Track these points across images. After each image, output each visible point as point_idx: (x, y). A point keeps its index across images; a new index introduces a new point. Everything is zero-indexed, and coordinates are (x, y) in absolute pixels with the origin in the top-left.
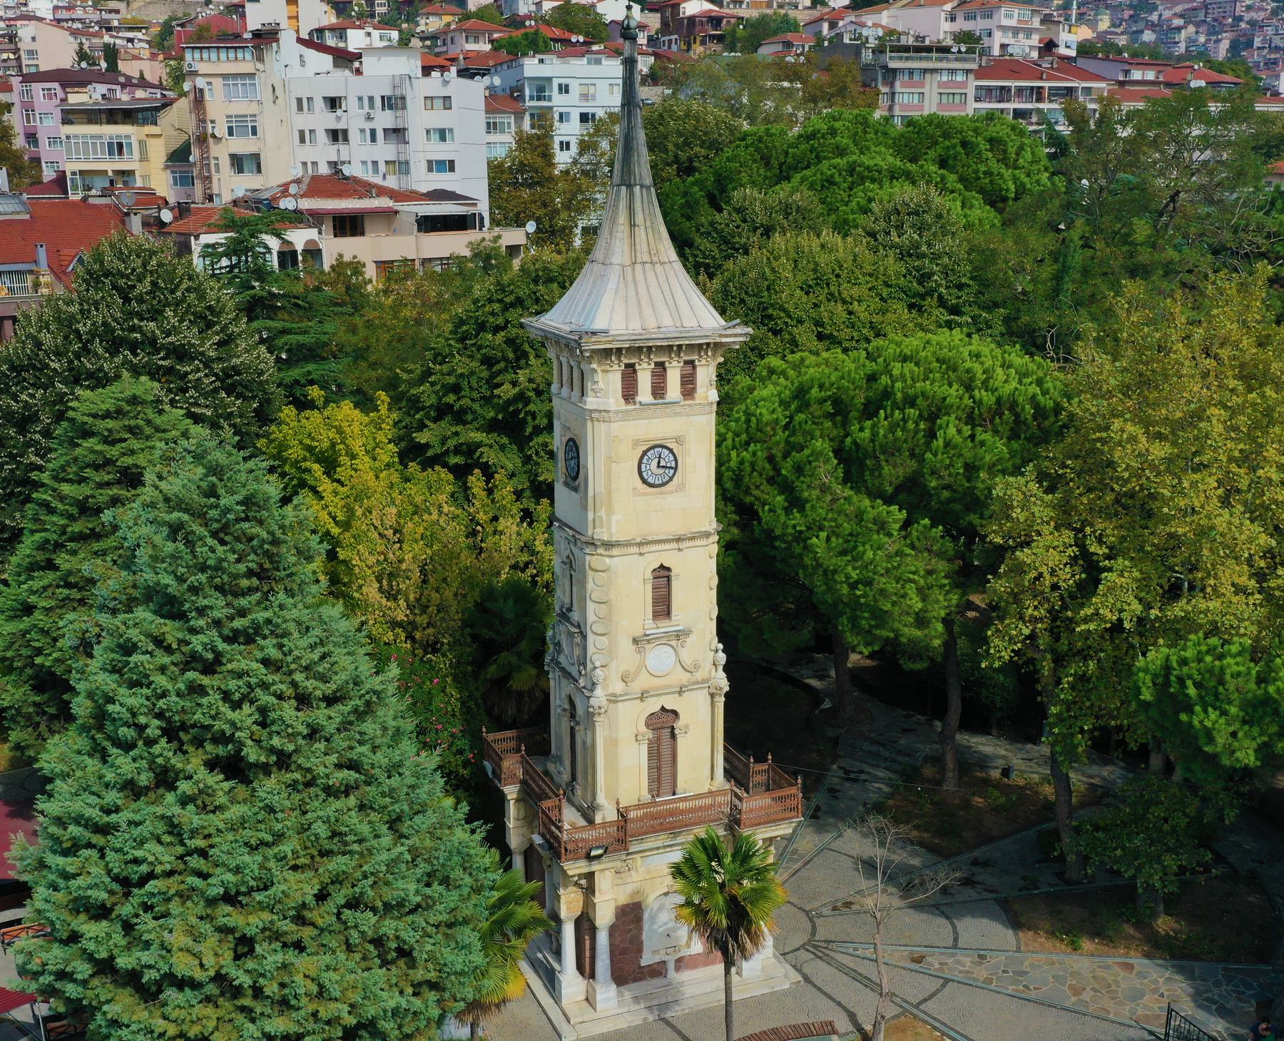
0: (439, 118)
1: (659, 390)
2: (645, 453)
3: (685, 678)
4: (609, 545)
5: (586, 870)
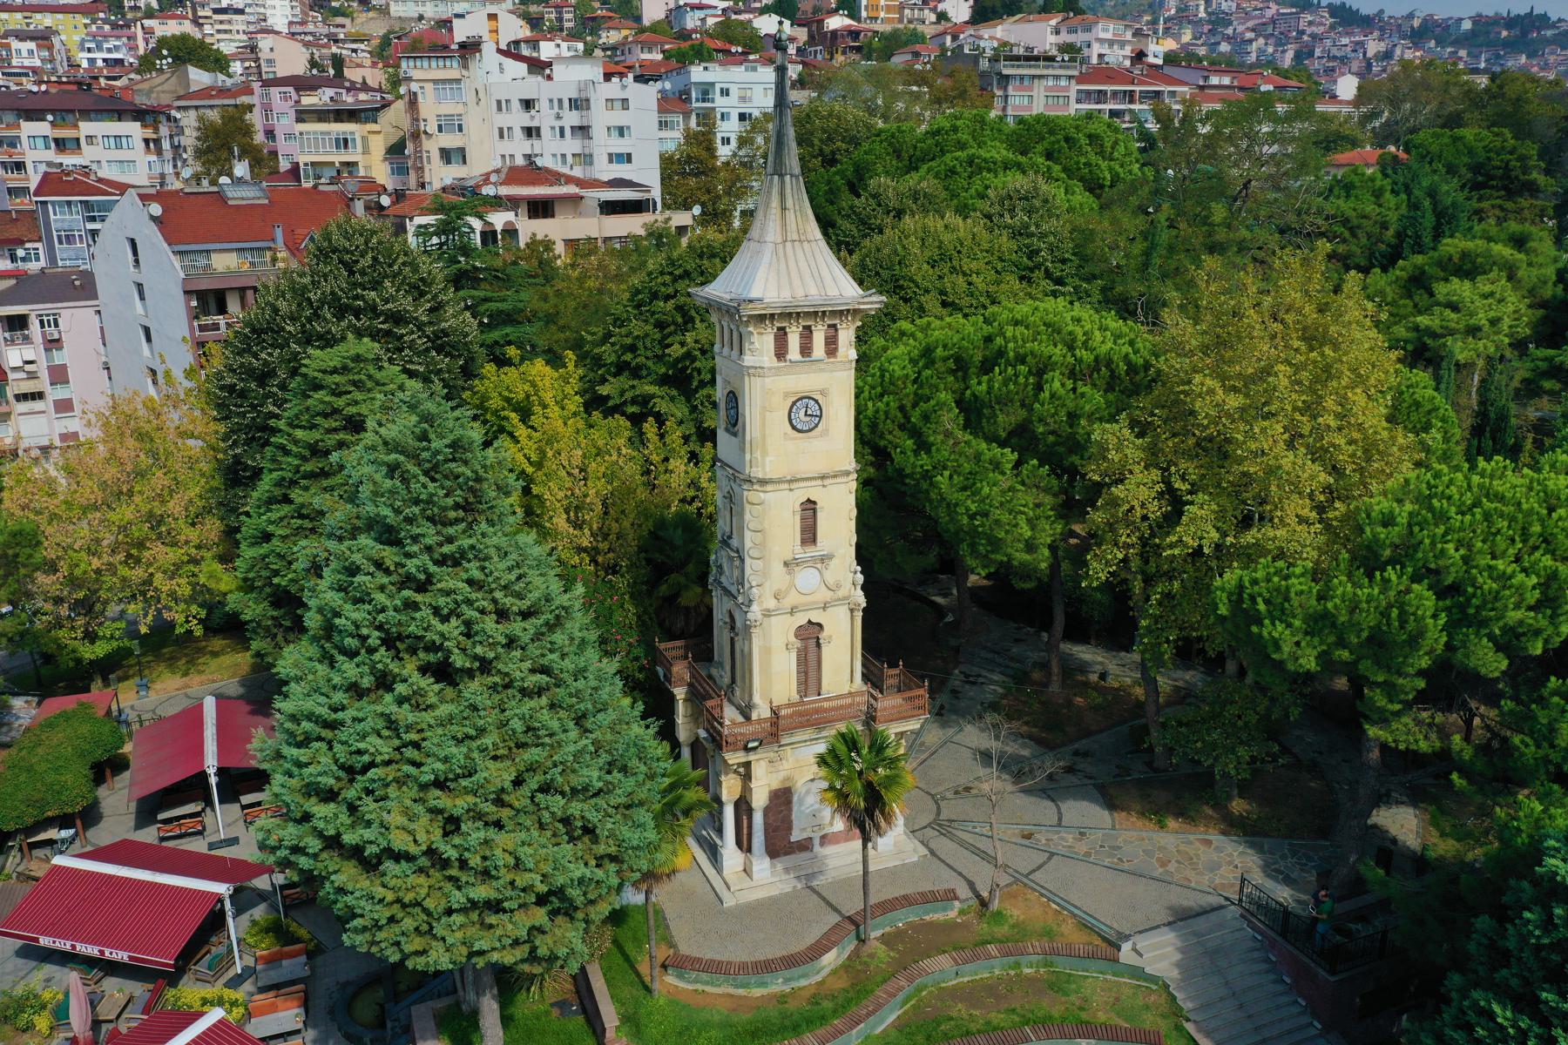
0: (618, 117)
1: (806, 350)
2: (794, 403)
3: (829, 595)
4: (763, 482)
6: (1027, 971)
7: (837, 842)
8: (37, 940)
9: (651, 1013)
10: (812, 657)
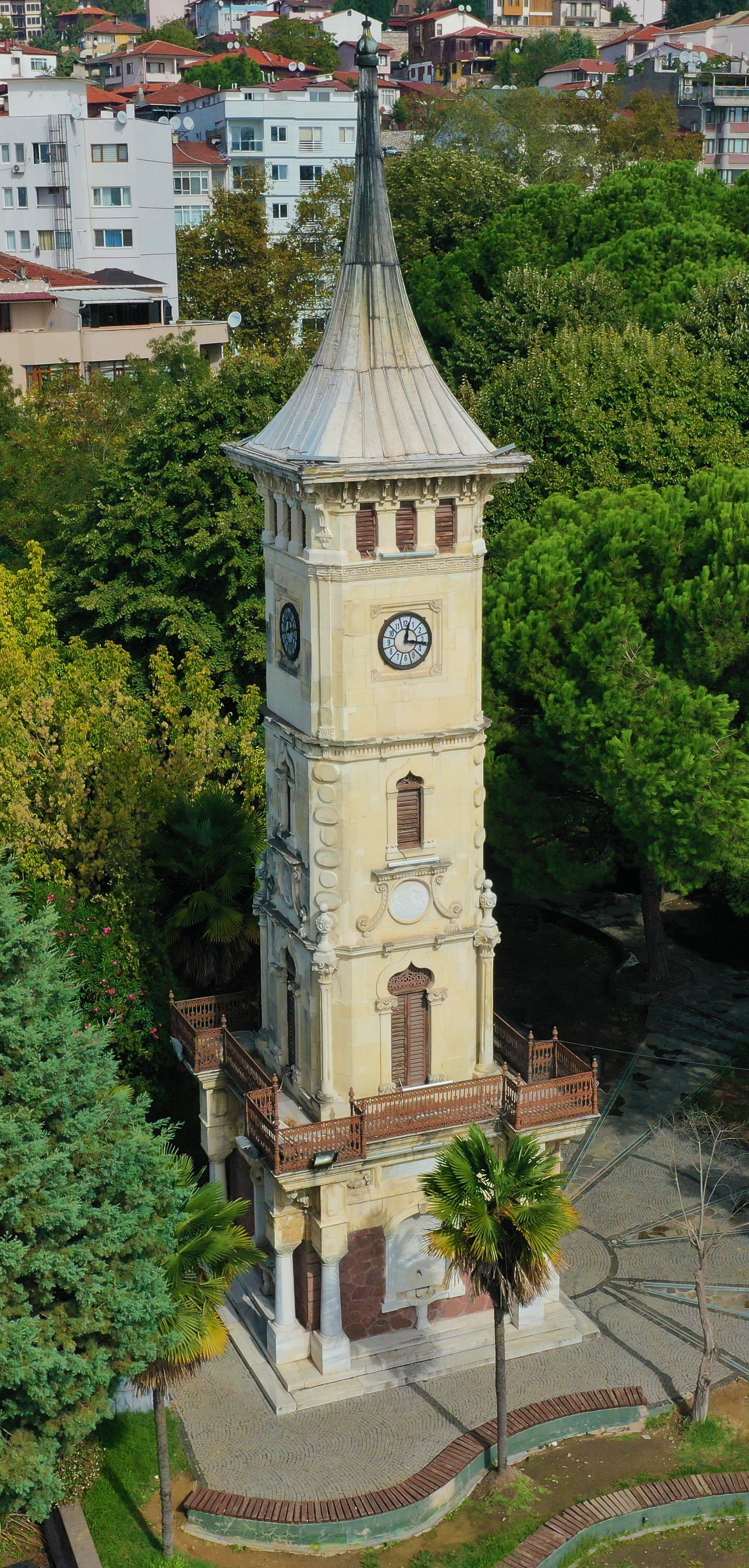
0: (111, 174)
1: (406, 538)
2: (387, 623)
5: (308, 1184)
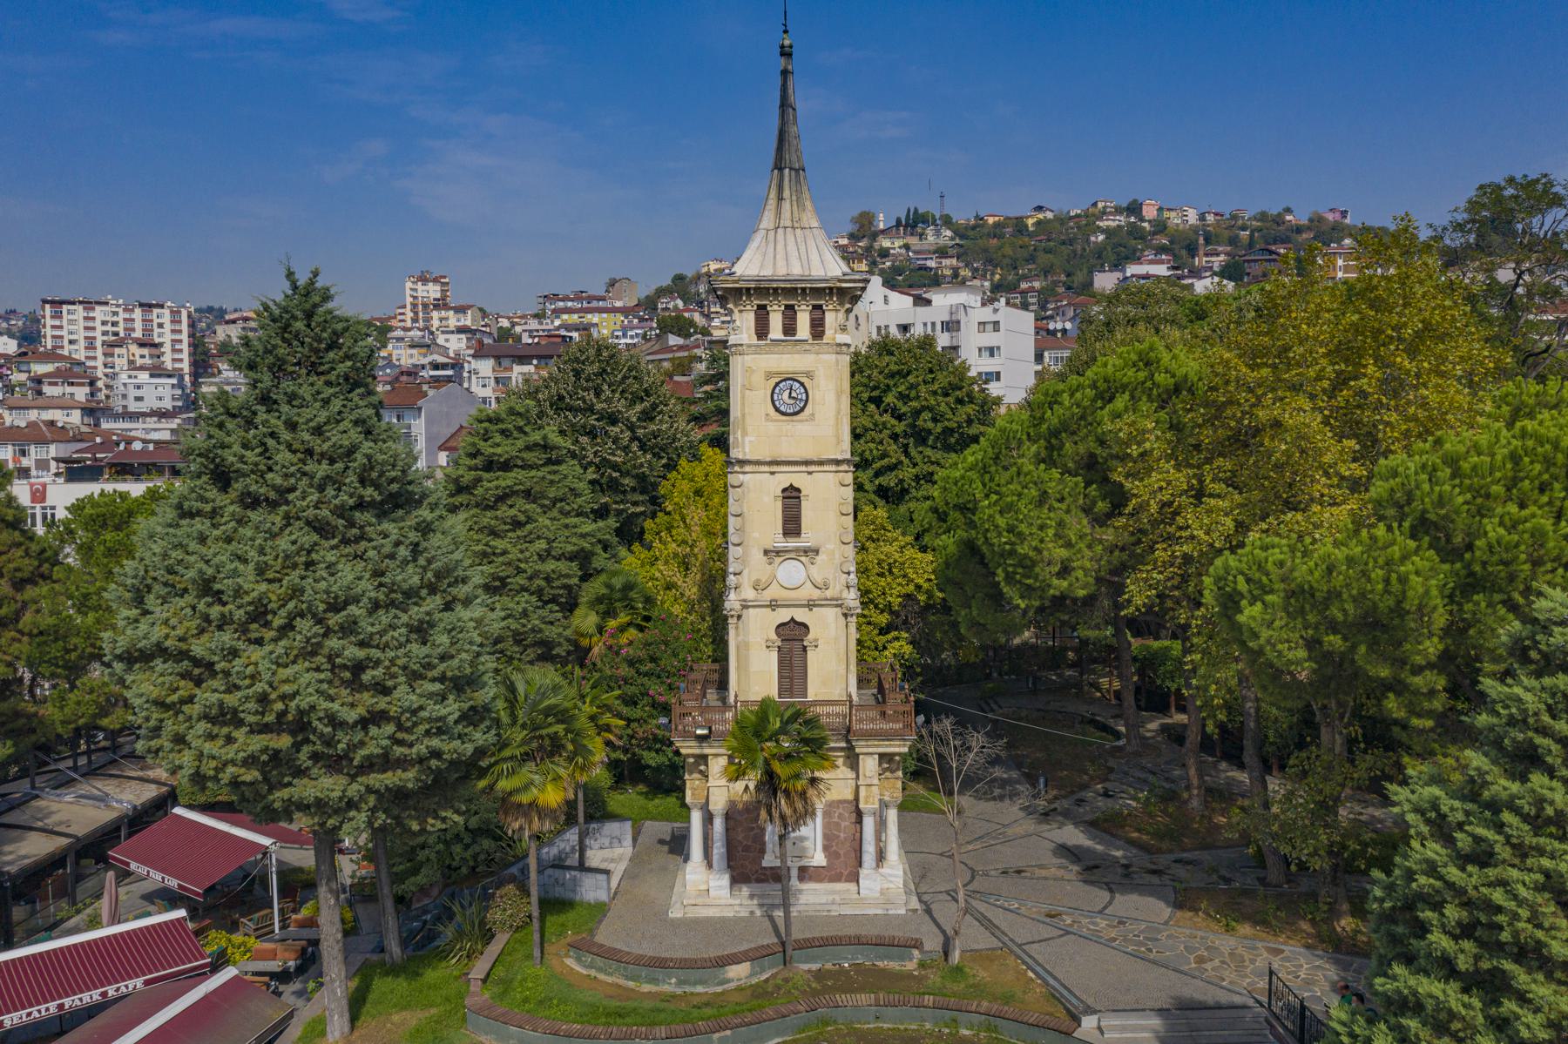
0: (990, 339)
1: (789, 329)
2: (777, 384)
3: (816, 594)
4: (742, 463)
5: (697, 751)
6: (966, 1032)
7: (820, 881)
8: (128, 864)
9: (525, 980)
10: (797, 661)
